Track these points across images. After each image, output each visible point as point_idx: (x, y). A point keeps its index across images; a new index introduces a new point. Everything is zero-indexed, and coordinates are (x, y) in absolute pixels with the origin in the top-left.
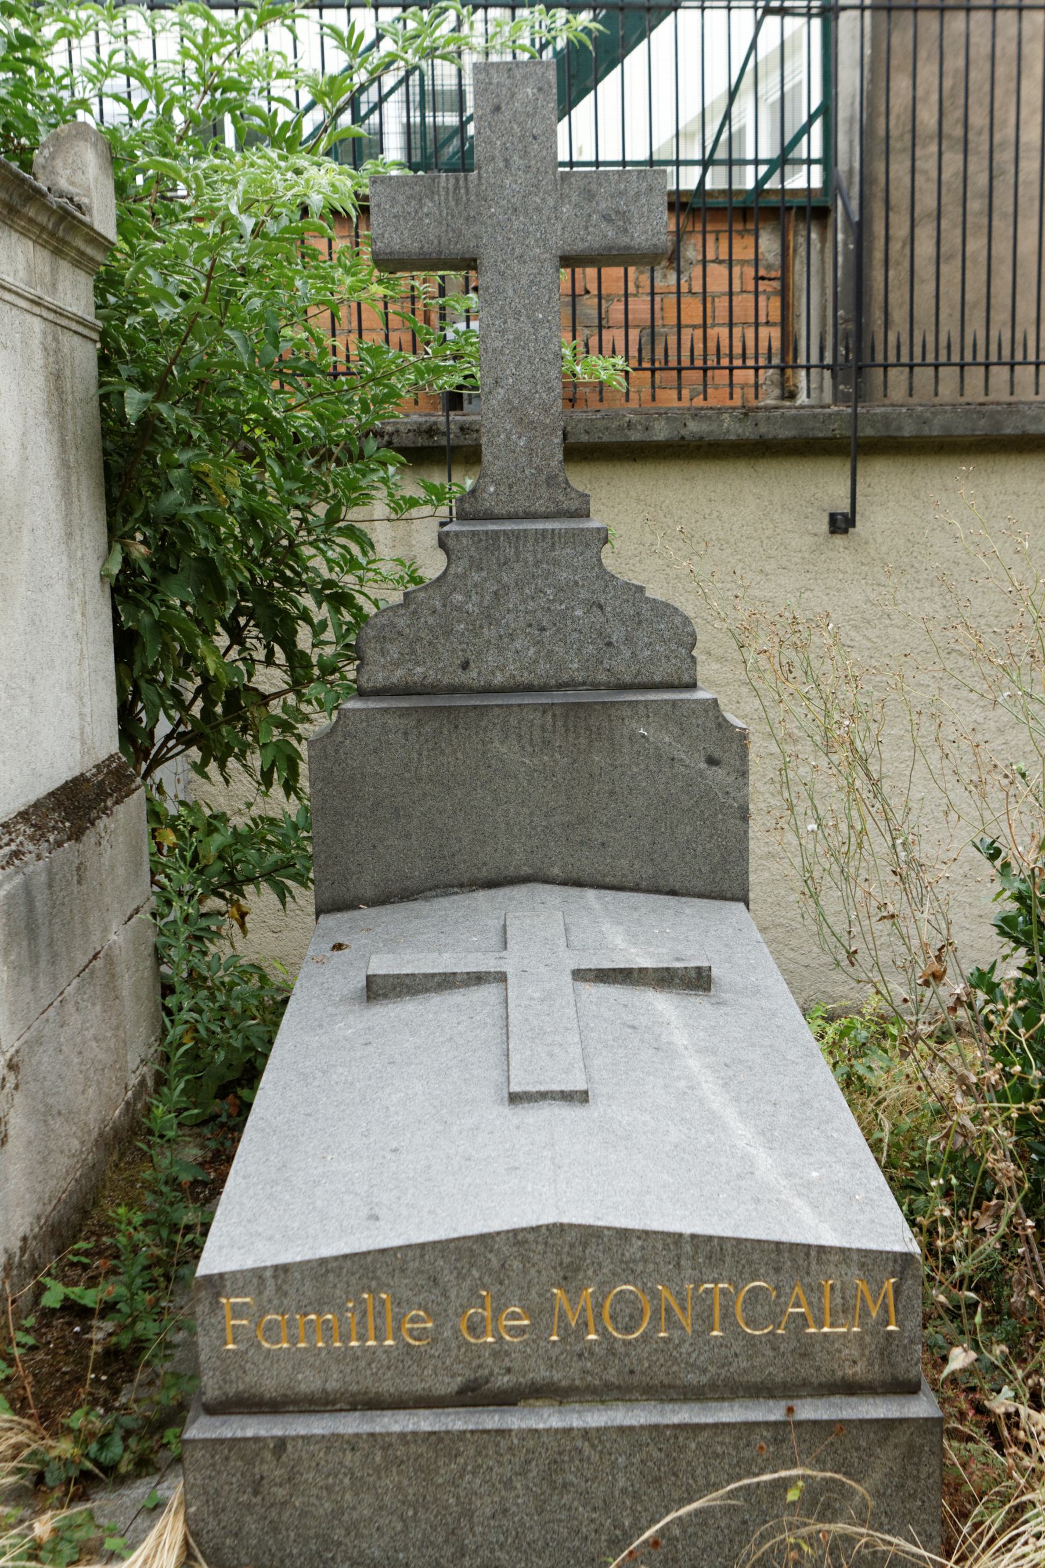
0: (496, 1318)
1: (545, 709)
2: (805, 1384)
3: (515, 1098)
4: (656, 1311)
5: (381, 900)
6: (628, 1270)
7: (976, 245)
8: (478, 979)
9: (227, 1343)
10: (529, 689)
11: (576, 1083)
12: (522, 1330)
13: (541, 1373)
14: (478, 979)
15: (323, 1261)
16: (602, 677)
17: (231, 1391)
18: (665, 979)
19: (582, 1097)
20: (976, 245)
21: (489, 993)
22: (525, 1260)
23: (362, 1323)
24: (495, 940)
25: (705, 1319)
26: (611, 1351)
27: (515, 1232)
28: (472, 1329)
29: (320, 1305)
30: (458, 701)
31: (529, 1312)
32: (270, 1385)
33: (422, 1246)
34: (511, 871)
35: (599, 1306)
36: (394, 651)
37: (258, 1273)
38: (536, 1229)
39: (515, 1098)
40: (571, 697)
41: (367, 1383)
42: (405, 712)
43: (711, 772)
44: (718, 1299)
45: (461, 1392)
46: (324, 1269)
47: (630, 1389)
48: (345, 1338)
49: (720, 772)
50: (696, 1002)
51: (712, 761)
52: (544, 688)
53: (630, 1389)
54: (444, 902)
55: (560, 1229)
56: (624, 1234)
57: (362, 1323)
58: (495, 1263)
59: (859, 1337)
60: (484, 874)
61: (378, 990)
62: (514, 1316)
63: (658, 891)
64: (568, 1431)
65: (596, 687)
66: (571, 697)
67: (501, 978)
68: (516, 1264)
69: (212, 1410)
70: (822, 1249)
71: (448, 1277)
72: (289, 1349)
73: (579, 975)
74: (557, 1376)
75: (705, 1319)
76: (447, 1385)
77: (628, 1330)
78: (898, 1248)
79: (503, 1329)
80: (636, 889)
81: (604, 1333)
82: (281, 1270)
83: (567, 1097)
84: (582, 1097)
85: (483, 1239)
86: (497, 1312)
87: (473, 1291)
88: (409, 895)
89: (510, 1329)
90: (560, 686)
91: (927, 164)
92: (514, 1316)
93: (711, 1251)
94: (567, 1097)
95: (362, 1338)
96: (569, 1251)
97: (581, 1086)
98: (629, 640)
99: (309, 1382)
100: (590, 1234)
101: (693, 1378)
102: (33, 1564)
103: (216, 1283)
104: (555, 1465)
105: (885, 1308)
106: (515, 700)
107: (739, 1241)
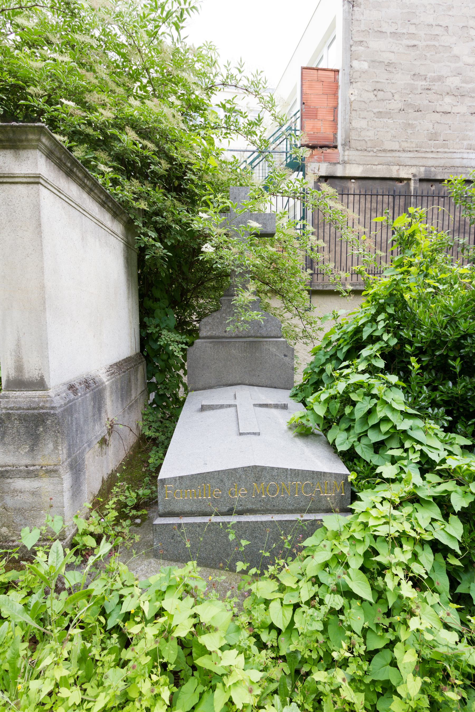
0: (238, 491)
1: (245, 342)
2: (320, 509)
3: (241, 434)
4: (281, 490)
5: (204, 389)
6: (273, 478)
7: (338, 248)
8: (230, 406)
9: (165, 498)
10: (241, 337)
11: (257, 431)
12: (245, 494)
13: (249, 506)
14: (230, 406)
15: (192, 475)
16: (259, 335)
17: (166, 510)
18: (276, 406)
19: (259, 434)
20: (338, 248)
21: (233, 409)
22: (246, 475)
23: (202, 492)
24: (233, 397)
25: (293, 492)
26: (268, 500)
27: (243, 468)
28: (231, 494)
29: (191, 487)
30: (224, 340)
31: (247, 489)
32: (177, 509)
33: (219, 471)
34: (236, 382)
35: (266, 488)
36: (208, 328)
37: (175, 479)
38: (249, 467)
39: (241, 434)
40: (251, 339)
41: (203, 508)
42: (211, 342)
43: (285, 358)
44: (297, 486)
45: (228, 511)
46: (192, 477)
47: (273, 510)
48: (197, 496)
49: (287, 358)
50: (284, 412)
51: (285, 356)
52: (245, 337)
53: (273, 510)
54: (220, 389)
55: (256, 467)
56: (272, 468)
57: (202, 492)
58: (238, 476)
59: (335, 497)
60: (229, 382)
61: (203, 408)
62: (243, 490)
63: (271, 387)
64: (257, 522)
65: (257, 337)
66: (251, 339)
67: (236, 406)
68: (244, 476)
69: (161, 516)
70: (324, 473)
71: (225, 480)
72: (182, 501)
73: (255, 405)
74: (254, 507)
75: (293, 492)
76: (225, 509)
77: (273, 494)
78: (344, 473)
79: (239, 495)
80: (266, 387)
81: (267, 495)
82: (181, 478)
83: (254, 434)
84: (259, 434)
85: (235, 469)
86: (238, 489)
87: (232, 484)
88: (210, 387)
89: (242, 494)
90: (249, 337)
91: (327, 230)
92: (243, 490)
93: (296, 473)
94: (254, 434)
95: (202, 496)
96: (257, 473)
97: (258, 431)
98: (265, 326)
99: (187, 508)
100: (263, 469)
101: (290, 507)
102: (234, 700)
103: (163, 481)
104: (253, 531)
105: (341, 489)
106: (238, 340)
107: (303, 471)
